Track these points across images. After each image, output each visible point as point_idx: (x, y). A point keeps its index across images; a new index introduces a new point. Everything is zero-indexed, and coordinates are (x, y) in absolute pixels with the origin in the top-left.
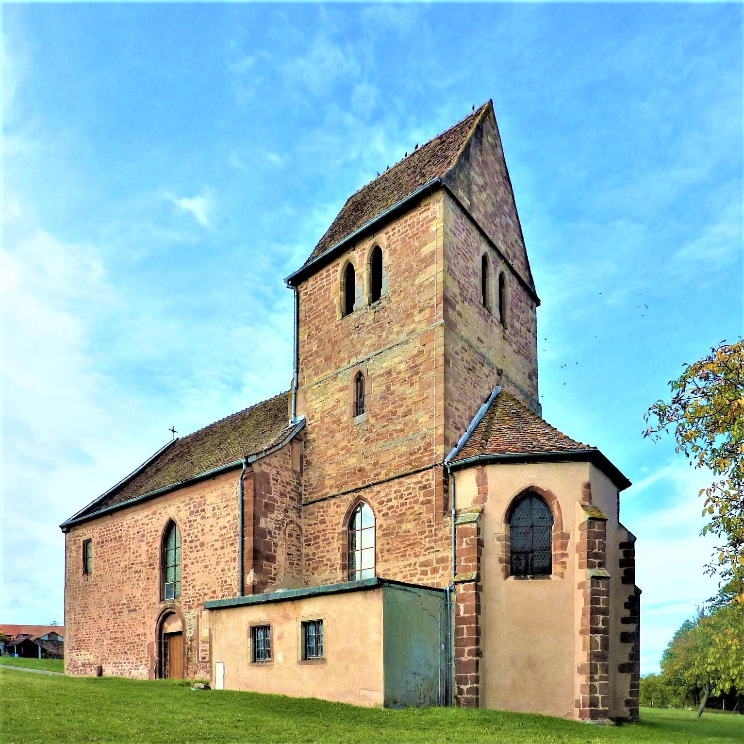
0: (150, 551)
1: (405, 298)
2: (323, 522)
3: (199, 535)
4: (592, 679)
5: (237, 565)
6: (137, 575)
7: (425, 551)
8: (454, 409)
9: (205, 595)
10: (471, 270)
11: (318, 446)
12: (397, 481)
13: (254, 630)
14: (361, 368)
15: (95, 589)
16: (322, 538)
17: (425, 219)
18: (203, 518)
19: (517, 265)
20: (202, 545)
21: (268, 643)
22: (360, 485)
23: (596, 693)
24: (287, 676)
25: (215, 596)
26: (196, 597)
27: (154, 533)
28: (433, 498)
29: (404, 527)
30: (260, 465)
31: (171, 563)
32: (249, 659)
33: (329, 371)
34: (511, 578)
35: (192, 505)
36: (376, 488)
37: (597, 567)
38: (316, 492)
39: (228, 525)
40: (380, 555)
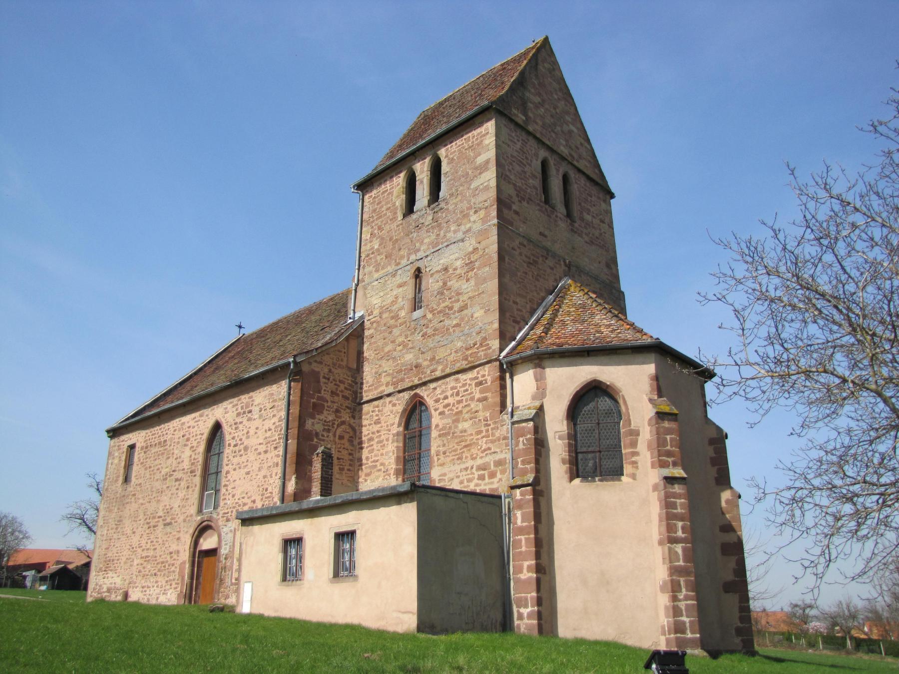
0: (193, 457)
1: (461, 201)
2: (378, 422)
3: (244, 438)
4: (674, 599)
5: (279, 470)
6: (177, 483)
7: (482, 452)
8: (511, 303)
9: (245, 504)
10: (528, 174)
12: (453, 377)
14: (420, 264)
16: (376, 440)
17: (478, 134)
18: (249, 419)
19: (582, 164)
22: (416, 382)
23: (682, 616)
24: (319, 599)
26: (234, 507)
27: (199, 437)
28: (489, 395)
29: (462, 426)
30: (310, 363)
32: (279, 577)
33: (389, 268)
34: (577, 481)
36: (432, 385)
37: (671, 467)
39: (273, 427)
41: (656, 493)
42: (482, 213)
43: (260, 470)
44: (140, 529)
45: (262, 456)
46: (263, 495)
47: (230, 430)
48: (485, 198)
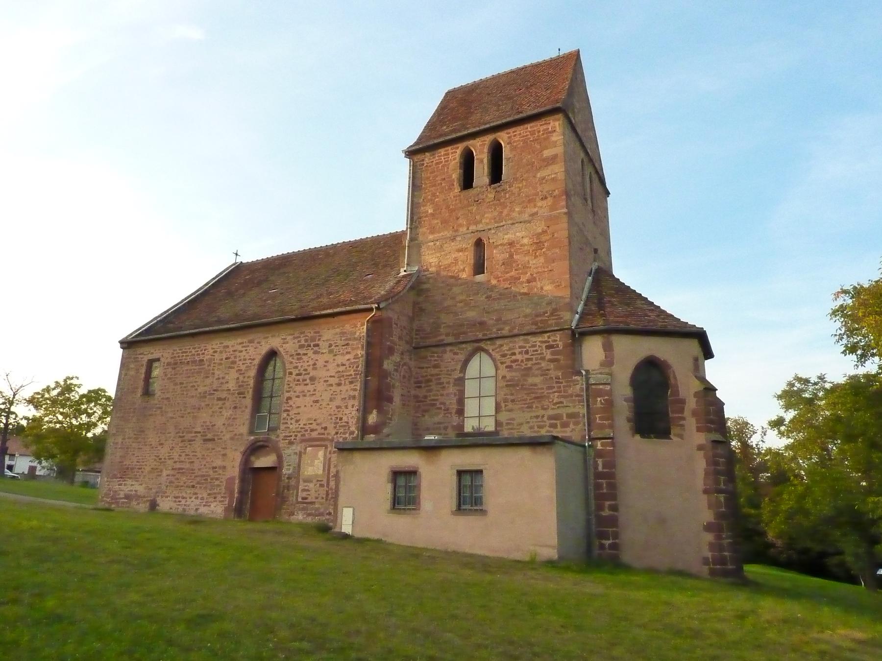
0: (241, 378)
2: (436, 366)
6: (220, 403)
9: (312, 430)
12: (522, 338)
13: (396, 474)
18: (315, 353)
19: (597, 165)
20: (312, 379)
21: (409, 489)
22: (480, 336)
24: (434, 522)
27: (248, 362)
29: (531, 380)
31: (266, 394)
32: (388, 505)
36: (499, 342)
40: (503, 405)
41: (702, 452)
42: (550, 201)
43: (331, 400)
45: (334, 388)
46: (336, 423)
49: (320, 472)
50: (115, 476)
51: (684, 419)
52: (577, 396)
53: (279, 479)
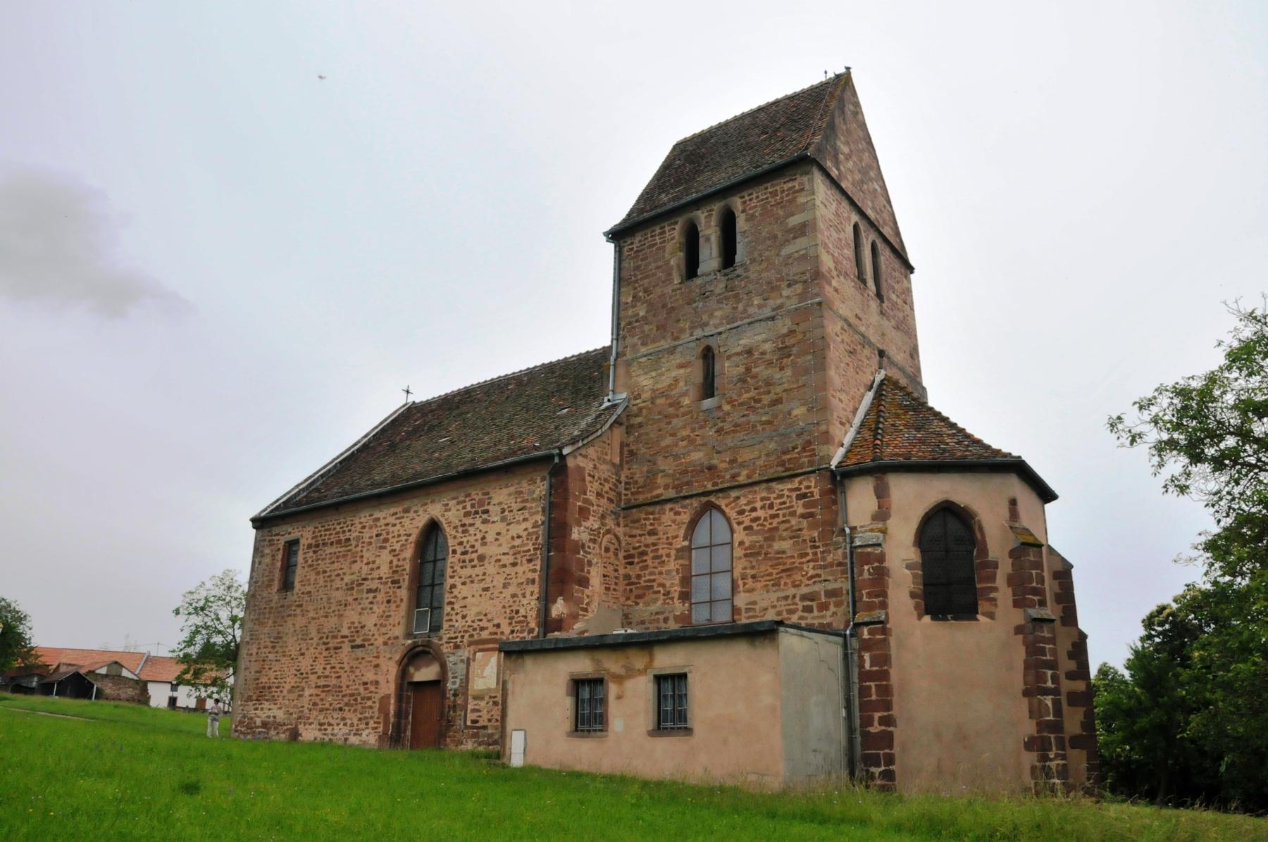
0: (395, 562)
1: (767, 269)
2: (652, 533)
3: (478, 545)
6: (371, 595)
9: (482, 629)
11: (647, 434)
12: (764, 486)
13: (577, 684)
15: (298, 611)
16: (651, 555)
17: (790, 189)
18: (485, 522)
19: (887, 231)
20: (481, 558)
22: (709, 487)
25: (499, 631)
26: (466, 632)
27: (403, 538)
29: (777, 546)
32: (568, 725)
33: (662, 342)
35: (468, 505)
36: (734, 494)
38: (642, 493)
40: (740, 583)
41: (1020, 637)
43: (505, 586)
44: (312, 650)
45: (508, 570)
46: (511, 618)
47: (454, 532)
48: (802, 269)
49: (493, 685)
50: (249, 699)
51: (995, 589)
52: (840, 564)
53: (443, 696)
